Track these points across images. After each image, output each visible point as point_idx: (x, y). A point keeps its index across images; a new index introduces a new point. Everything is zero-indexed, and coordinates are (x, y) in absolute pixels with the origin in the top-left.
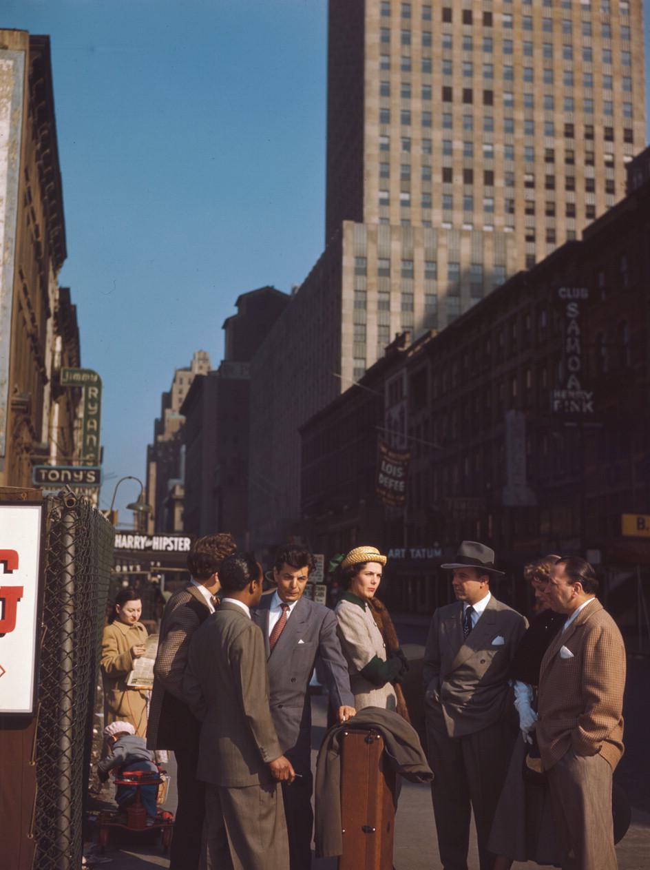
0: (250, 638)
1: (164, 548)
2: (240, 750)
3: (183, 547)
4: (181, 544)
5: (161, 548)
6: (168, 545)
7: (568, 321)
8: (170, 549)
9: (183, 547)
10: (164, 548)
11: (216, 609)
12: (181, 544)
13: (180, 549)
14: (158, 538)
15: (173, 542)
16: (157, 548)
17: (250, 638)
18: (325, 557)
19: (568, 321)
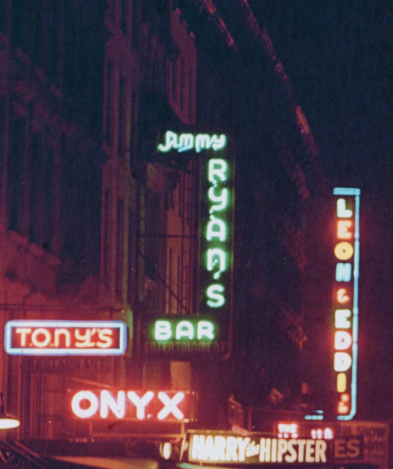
0: (182, 262)
1: (280, 460)
2: (42, 314)
3: (313, 455)
4: (310, 451)
5: (274, 460)
6: (288, 453)
7: (207, 278)
8: (290, 459)
9: (313, 455)
10: (280, 460)
11: (11, 357)
12: (310, 451)
13: (309, 459)
14: (269, 440)
15: (296, 447)
16: (268, 460)
17: (182, 262)
18: (12, 317)
19: (207, 278)
